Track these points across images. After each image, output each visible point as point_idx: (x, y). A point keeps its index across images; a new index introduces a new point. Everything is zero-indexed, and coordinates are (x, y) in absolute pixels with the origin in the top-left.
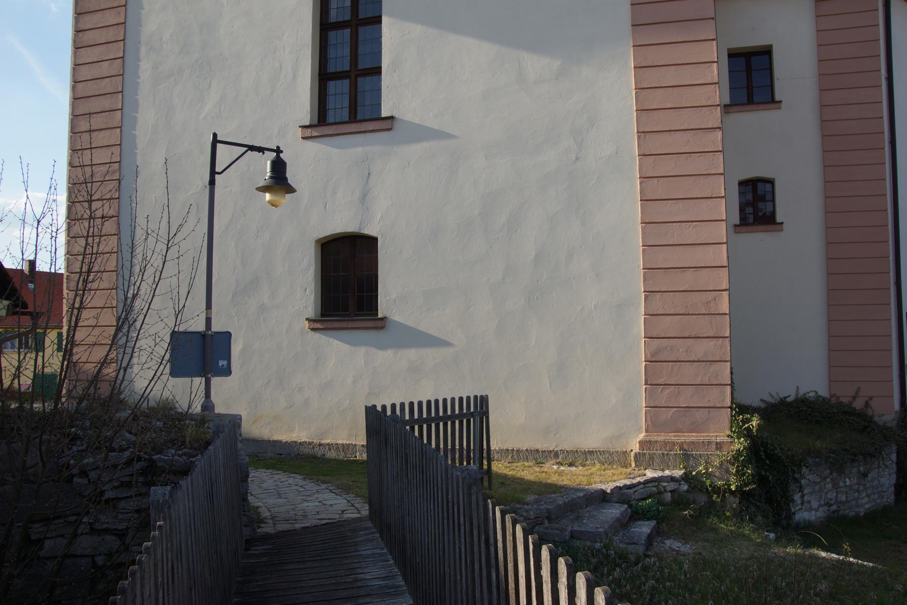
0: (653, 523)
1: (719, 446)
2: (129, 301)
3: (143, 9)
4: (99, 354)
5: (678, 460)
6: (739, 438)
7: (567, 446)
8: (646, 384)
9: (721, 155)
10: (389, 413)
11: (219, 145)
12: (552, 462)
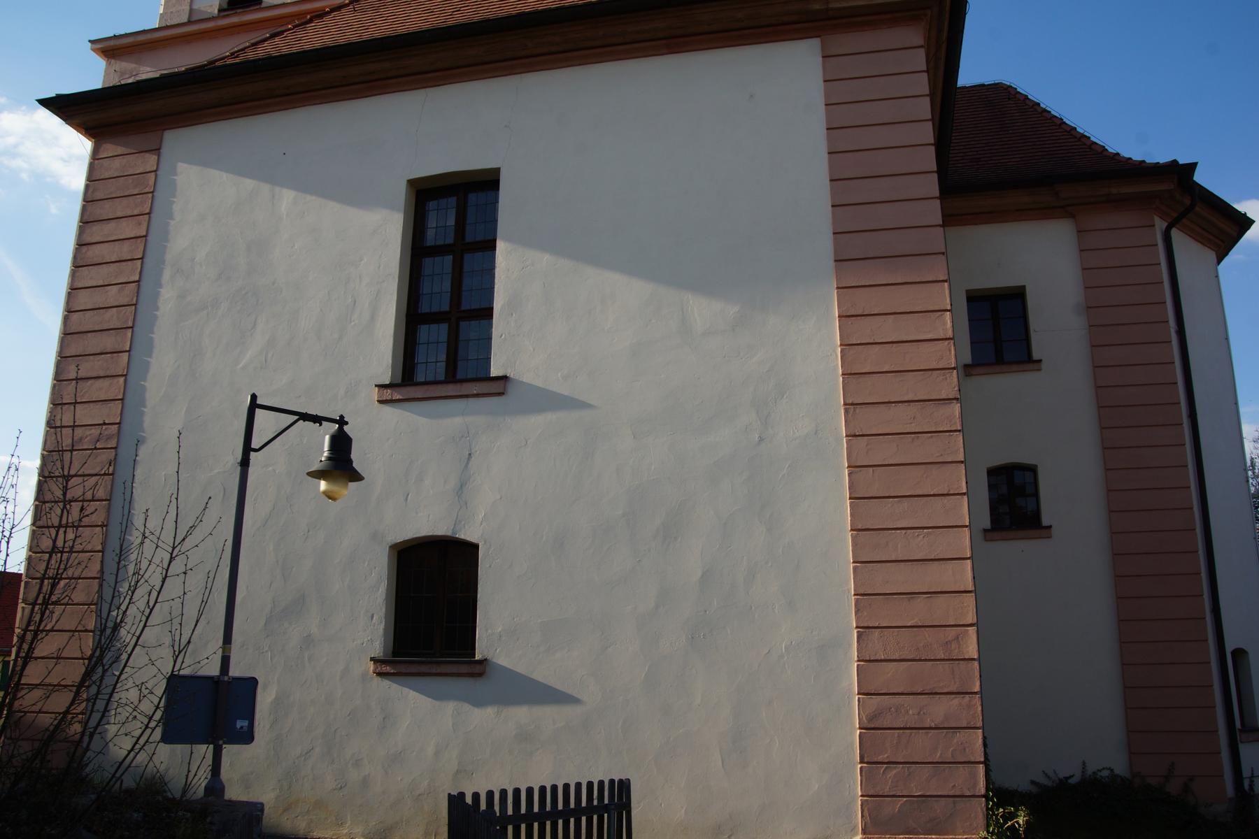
2: (108, 631)
3: (172, 218)
4: (60, 702)
10: (483, 806)
11: (258, 411)
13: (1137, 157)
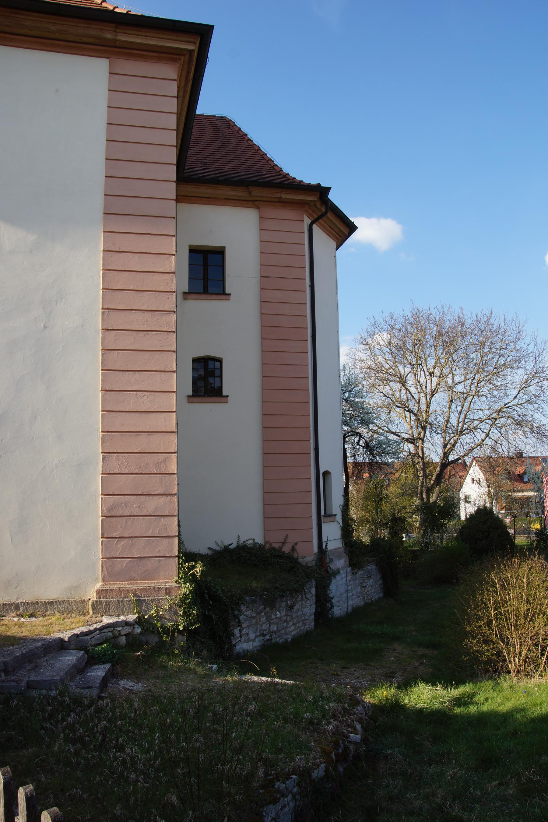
0: (108, 666)
1: (168, 591)
5: (132, 606)
6: (185, 583)
7: (28, 598)
8: (103, 537)
9: (174, 335)
12: (13, 615)
13: (299, 178)
